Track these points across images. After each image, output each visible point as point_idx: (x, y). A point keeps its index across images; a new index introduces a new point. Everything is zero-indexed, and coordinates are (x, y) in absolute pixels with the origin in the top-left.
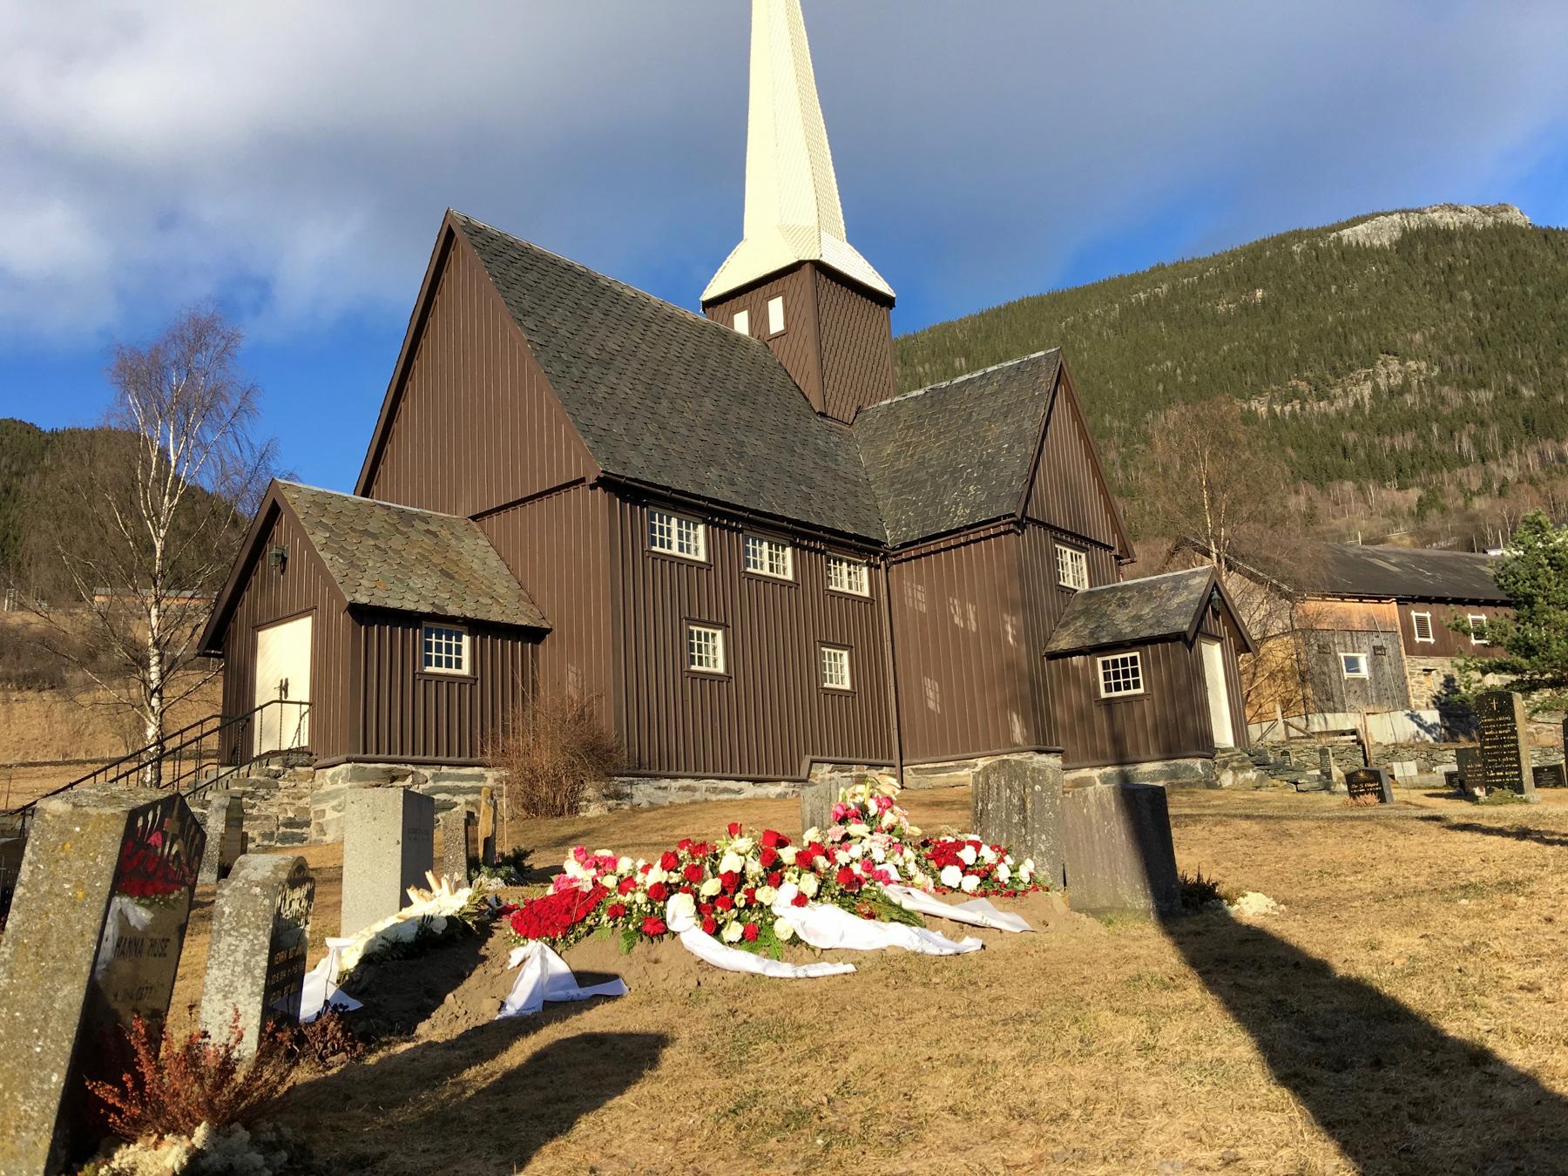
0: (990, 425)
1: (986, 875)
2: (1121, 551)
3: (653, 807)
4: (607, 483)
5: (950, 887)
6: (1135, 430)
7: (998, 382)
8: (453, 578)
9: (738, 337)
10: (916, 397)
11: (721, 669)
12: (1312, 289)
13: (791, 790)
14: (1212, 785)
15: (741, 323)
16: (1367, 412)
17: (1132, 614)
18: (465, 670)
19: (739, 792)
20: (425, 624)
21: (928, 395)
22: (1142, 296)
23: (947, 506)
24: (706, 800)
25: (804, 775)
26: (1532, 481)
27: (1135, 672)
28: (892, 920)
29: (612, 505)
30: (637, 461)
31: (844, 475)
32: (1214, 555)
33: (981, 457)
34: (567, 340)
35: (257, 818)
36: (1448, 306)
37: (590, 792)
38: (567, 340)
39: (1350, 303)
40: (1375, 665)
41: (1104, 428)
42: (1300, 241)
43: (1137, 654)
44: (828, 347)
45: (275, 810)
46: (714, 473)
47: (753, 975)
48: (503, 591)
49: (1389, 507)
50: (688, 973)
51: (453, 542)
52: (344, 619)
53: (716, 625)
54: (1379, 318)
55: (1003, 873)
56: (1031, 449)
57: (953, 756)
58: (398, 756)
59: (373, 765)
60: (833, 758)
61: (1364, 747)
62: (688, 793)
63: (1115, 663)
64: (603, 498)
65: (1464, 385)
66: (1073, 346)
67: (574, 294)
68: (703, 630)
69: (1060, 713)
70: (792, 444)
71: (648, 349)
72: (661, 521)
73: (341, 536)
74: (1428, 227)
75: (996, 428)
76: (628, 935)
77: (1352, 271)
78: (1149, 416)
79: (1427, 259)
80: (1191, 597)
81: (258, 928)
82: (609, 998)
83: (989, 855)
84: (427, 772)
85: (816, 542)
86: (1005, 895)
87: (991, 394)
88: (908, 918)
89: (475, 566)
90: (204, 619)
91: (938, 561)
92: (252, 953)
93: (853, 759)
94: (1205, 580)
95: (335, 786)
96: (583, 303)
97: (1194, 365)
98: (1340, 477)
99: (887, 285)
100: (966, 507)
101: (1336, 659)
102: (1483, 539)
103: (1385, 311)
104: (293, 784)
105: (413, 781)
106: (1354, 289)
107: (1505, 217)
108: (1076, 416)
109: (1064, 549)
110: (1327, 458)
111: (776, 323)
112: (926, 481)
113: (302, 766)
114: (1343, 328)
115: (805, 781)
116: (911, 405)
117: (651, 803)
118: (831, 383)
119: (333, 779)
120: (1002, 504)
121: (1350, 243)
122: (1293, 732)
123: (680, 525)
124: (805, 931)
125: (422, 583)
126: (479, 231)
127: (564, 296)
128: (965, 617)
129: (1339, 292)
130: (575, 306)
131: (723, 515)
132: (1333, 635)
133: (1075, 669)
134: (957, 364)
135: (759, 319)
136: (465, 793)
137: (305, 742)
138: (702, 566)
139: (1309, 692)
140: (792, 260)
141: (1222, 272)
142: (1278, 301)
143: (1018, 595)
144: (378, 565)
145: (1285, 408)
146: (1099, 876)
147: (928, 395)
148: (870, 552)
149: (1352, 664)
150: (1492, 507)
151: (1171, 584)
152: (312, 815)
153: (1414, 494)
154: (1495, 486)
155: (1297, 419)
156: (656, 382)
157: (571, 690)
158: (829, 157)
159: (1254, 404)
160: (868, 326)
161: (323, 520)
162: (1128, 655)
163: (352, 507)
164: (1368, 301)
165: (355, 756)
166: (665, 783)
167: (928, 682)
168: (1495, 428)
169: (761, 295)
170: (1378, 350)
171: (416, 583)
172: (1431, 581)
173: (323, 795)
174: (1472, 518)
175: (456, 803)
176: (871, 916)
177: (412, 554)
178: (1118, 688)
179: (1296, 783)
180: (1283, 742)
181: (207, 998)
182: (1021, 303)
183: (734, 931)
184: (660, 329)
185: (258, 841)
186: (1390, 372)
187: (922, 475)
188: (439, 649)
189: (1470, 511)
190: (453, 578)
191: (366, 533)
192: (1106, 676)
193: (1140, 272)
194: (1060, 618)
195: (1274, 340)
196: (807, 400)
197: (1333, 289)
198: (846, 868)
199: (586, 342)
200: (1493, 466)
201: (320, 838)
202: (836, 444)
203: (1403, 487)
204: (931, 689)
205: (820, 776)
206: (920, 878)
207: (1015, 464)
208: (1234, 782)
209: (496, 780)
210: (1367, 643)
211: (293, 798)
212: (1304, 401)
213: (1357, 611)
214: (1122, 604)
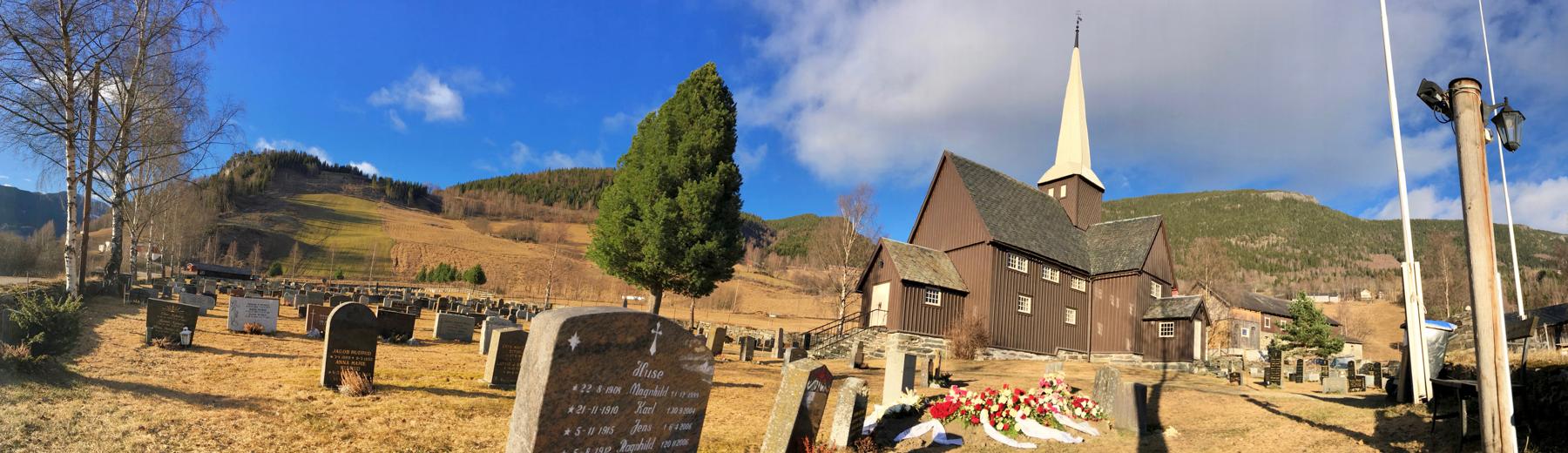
1: (1088, 413)
4: (994, 244)
9: (1049, 197)
11: (1029, 312)
15: (1051, 193)
18: (939, 304)
25: (1055, 354)
29: (994, 252)
30: (1005, 236)
39: (1265, 215)
40: (1252, 333)
46: (1034, 243)
47: (1004, 445)
50: (983, 440)
52: (900, 284)
53: (1029, 296)
55: (1094, 412)
65: (1293, 247)
76: (966, 422)
78: (1196, 239)
82: (957, 446)
83: (1090, 405)
84: (924, 338)
88: (1060, 427)
90: (858, 279)
91: (1109, 282)
92: (848, 412)
94: (1199, 299)
102: (1291, 295)
106: (1267, 211)
108: (1165, 238)
111: (1063, 193)
122: (1223, 354)
128: (1115, 303)
131: (1035, 257)
135: (1057, 192)
149: (1245, 332)
153: (1275, 278)
157: (975, 315)
166: (1005, 351)
171: (925, 273)
172: (1272, 308)
174: (1289, 288)
176: (1047, 425)
183: (1000, 426)
186: (1273, 239)
198: (1041, 405)
203: (1271, 275)
204: (1100, 327)
206: (1068, 412)
210: (1251, 325)
212: (1247, 242)
213: (1249, 314)
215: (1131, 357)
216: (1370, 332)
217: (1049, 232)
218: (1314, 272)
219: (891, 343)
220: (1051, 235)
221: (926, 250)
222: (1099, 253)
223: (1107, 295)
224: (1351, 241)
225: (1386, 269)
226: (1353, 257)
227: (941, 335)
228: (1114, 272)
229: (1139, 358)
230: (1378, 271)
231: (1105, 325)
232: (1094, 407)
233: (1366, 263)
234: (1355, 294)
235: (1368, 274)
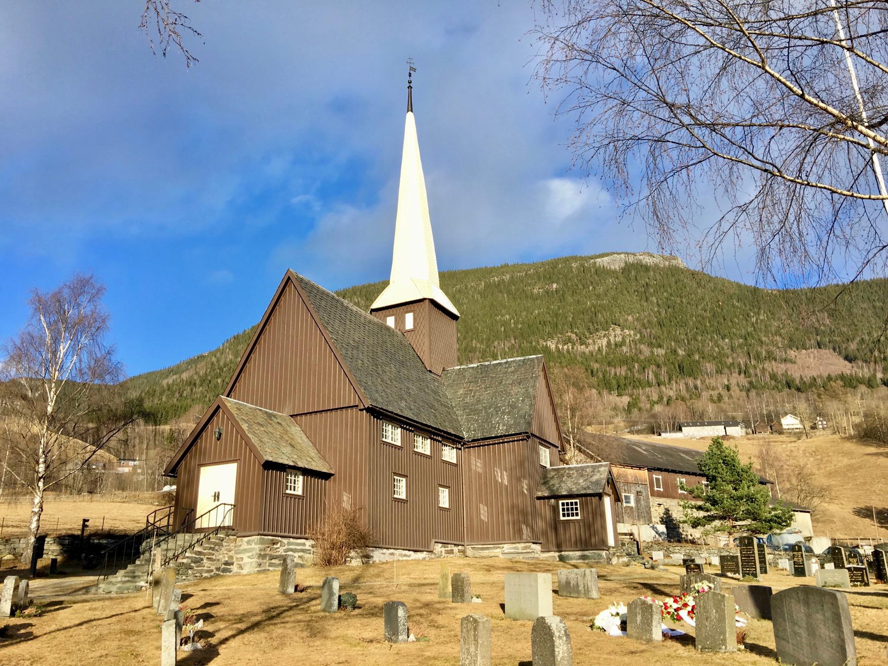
9: (388, 329)
10: (473, 368)
12: (580, 286)
15: (391, 322)
19: (409, 556)
22: (496, 279)
25: (431, 550)
26: (683, 399)
27: (577, 509)
29: (370, 419)
33: (509, 402)
35: (214, 560)
36: (645, 304)
39: (598, 296)
40: (638, 501)
41: (472, 347)
42: (576, 262)
45: (221, 556)
46: (403, 404)
51: (288, 428)
52: (258, 468)
60: (442, 541)
61: (637, 542)
63: (567, 504)
65: (651, 345)
68: (399, 478)
74: (637, 263)
75: (515, 389)
78: (496, 343)
79: (636, 279)
84: (285, 541)
87: (512, 372)
93: (449, 542)
95: (250, 547)
100: (504, 425)
102: (659, 427)
106: (601, 290)
107: (674, 262)
112: (482, 410)
116: (471, 371)
121: (600, 266)
135: (400, 321)
150: (664, 411)
152: (235, 560)
153: (626, 400)
154: (665, 399)
159: (549, 343)
162: (574, 501)
166: (385, 551)
167: (481, 506)
168: (664, 370)
177: (277, 435)
186: (616, 334)
187: (480, 407)
189: (653, 412)
192: (563, 510)
197: (591, 288)
200: (663, 388)
203: (620, 395)
204: (483, 510)
210: (634, 489)
213: (630, 472)
216: (823, 492)
218: (691, 385)
219: (245, 551)
222: (471, 410)
224: (750, 329)
225: (825, 375)
226: (758, 357)
227: (303, 535)
229: (538, 547)
230: (807, 380)
233: (783, 367)
234: (771, 423)
235: (789, 385)
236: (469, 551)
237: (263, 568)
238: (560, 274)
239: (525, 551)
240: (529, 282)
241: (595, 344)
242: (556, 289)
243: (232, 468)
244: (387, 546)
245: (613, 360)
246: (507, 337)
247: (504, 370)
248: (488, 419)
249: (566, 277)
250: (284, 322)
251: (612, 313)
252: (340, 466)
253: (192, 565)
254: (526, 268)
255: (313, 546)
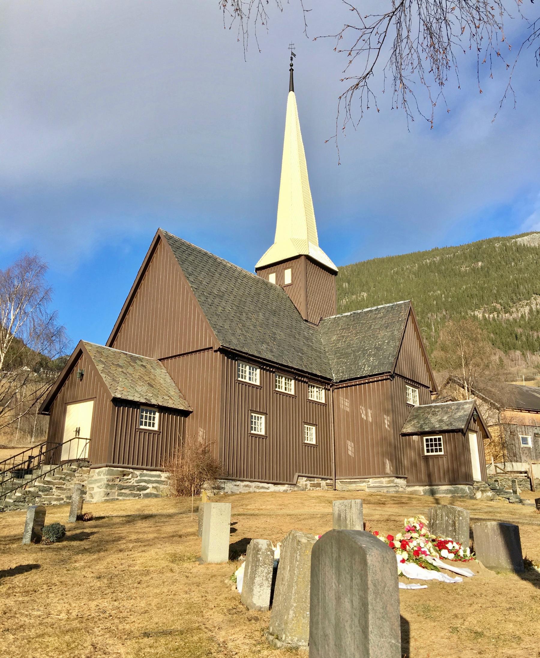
0: (379, 331)
2: (432, 389)
3: (233, 494)
4: (223, 351)
5: (444, 557)
6: (423, 321)
7: (383, 313)
8: (153, 387)
9: (272, 285)
10: (347, 316)
11: (263, 433)
12: (504, 263)
13: (290, 488)
14: (473, 498)
15: (272, 278)
16: (527, 320)
17: (439, 419)
18: (156, 428)
19: (268, 488)
20: (142, 407)
21: (352, 315)
22: (428, 261)
23: (360, 366)
24: (255, 492)
25: (295, 482)
27: (440, 445)
28: (432, 569)
29: (224, 359)
30: (235, 341)
31: (315, 348)
32: (466, 388)
33: (376, 345)
34: (206, 286)
35: (65, 489)
37: (205, 486)
38: (206, 286)
39: (520, 271)
40: (535, 442)
42: (499, 242)
43: (441, 437)
44: (310, 291)
46: (265, 346)
48: (173, 393)
49: (536, 364)
51: (152, 370)
54: (533, 278)
56: (398, 344)
57: (359, 477)
58: (126, 465)
59: (116, 469)
60: (307, 475)
61: (530, 479)
62: (247, 488)
63: (431, 440)
64: (220, 356)
66: (396, 281)
67: (208, 266)
68: (257, 415)
69: (406, 462)
70: (295, 334)
71: (237, 291)
72: (242, 367)
73: (109, 367)
75: (382, 333)
77: (521, 257)
78: (429, 315)
80: (465, 413)
81: (269, 565)
83: (457, 547)
84: (138, 473)
85: (304, 378)
86: (463, 561)
87: (381, 318)
88: (436, 568)
89: (161, 382)
93: (315, 476)
94: (471, 406)
95: (99, 477)
96: (211, 269)
97: (450, 293)
98: (514, 348)
99: (335, 266)
100: (369, 367)
101: (518, 438)
103: (536, 275)
104: (81, 475)
105: (132, 477)
106: (522, 265)
108: (416, 329)
109: (409, 387)
110: (508, 340)
113: (85, 467)
114: (517, 281)
115: (295, 485)
116: (344, 319)
117: (232, 492)
118: (310, 307)
119: (99, 474)
120: (385, 367)
121: (521, 245)
122: (499, 471)
123: (250, 369)
124: (405, 572)
125: (141, 388)
126: (170, 238)
127: (204, 267)
129: (515, 266)
130: (208, 271)
131: (267, 365)
132: (517, 427)
133: (414, 441)
134: (344, 286)
135: (280, 277)
136: (152, 483)
137: (87, 457)
138: (258, 387)
139: (506, 452)
140: (296, 254)
141: (464, 253)
142: (488, 268)
143: (390, 407)
144: (124, 380)
145: (490, 316)
146: (491, 555)
147: (352, 315)
148: (326, 383)
149: (525, 440)
151: (456, 407)
152: (87, 489)
155: (495, 321)
156: (241, 305)
157: (200, 439)
158: (313, 211)
159: (476, 313)
160: (326, 283)
161: (102, 359)
162: (437, 437)
163: (112, 354)
164: (528, 270)
165: (109, 464)
166: (238, 483)
167: (349, 443)
169: (282, 268)
170: (532, 293)
173: (93, 481)
175: (148, 487)
176: (424, 568)
177: (136, 375)
178: (432, 451)
179: (509, 499)
180: (494, 475)
181: (255, 587)
182: (374, 260)
184: (242, 281)
185: (65, 500)
187: (349, 351)
188: (146, 419)
190: (153, 387)
191: (118, 365)
192: (427, 446)
193: (428, 250)
194: (407, 418)
195: (486, 285)
196: (300, 314)
197: (513, 264)
199: (213, 287)
201: (90, 500)
202: (312, 334)
204: (350, 446)
205: (301, 483)
207: (390, 349)
208: (482, 497)
209: (166, 478)
211: (80, 481)
212: (499, 313)
214: (434, 414)
215: (392, 482)
217: (278, 331)
219: (96, 481)
220: (281, 335)
221: (137, 358)
223: (355, 406)
227: (159, 468)
228: (361, 378)
229: (402, 482)
231: (356, 443)
232: (460, 548)
236: (339, 486)
237: (111, 498)
238: (484, 253)
239: (389, 485)
240: (457, 262)
241: (518, 312)
242: (481, 266)
243: (90, 405)
244: (242, 479)
245: (535, 325)
246: (439, 309)
247: (373, 317)
248: (355, 362)
249: (490, 256)
250: (155, 276)
251: (533, 284)
252: (197, 404)
253: (40, 493)
254: (454, 250)
255: (169, 478)
